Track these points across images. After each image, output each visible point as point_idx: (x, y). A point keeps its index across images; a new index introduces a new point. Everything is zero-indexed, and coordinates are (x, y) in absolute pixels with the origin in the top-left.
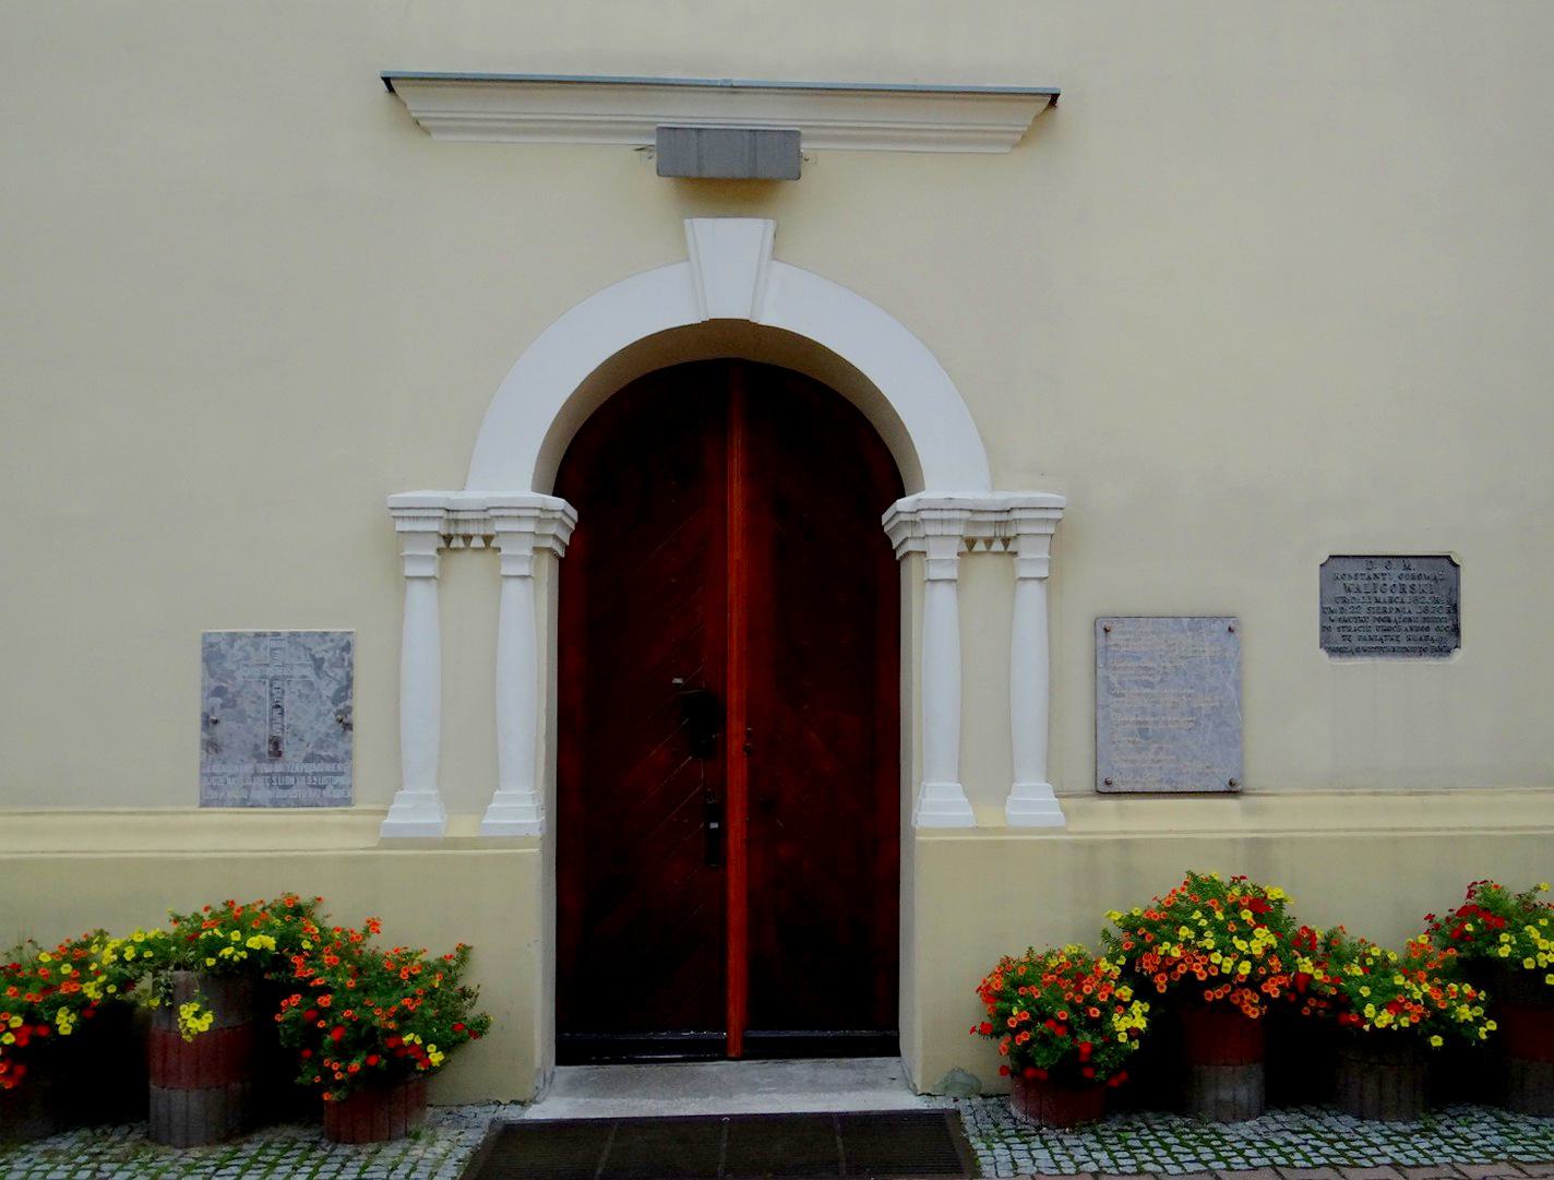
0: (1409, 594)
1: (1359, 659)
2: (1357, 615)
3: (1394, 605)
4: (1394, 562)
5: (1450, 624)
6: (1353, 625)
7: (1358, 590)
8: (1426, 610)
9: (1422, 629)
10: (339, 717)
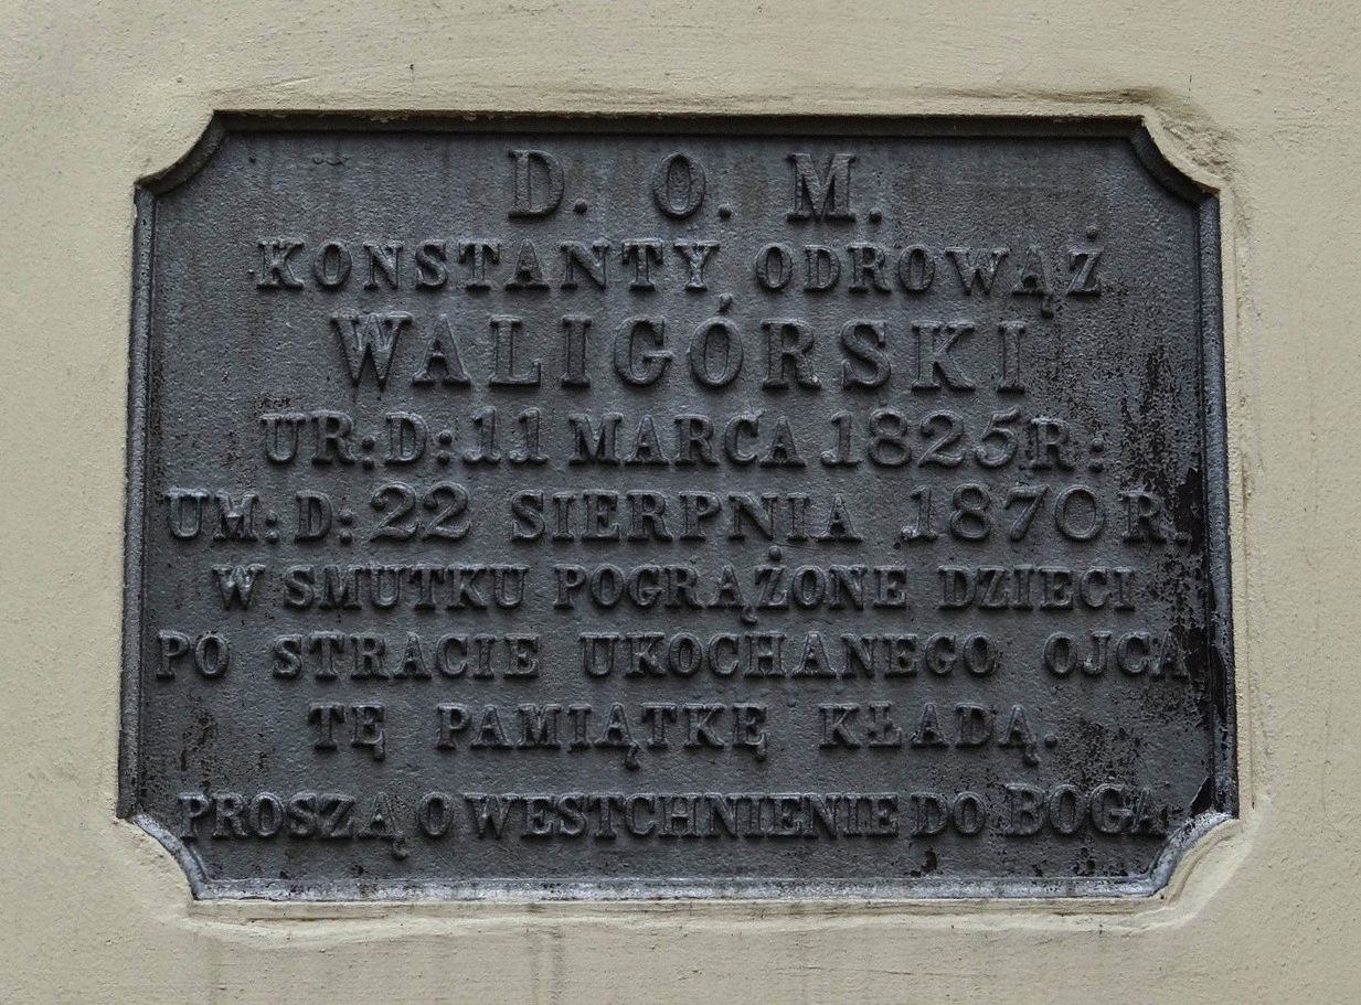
0: (835, 406)
1: (434, 894)
2: (426, 562)
3: (721, 490)
4: (718, 169)
5: (1153, 624)
6: (404, 637)
7: (443, 380)
8: (970, 528)
9: (941, 666)
10: (39, 765)
